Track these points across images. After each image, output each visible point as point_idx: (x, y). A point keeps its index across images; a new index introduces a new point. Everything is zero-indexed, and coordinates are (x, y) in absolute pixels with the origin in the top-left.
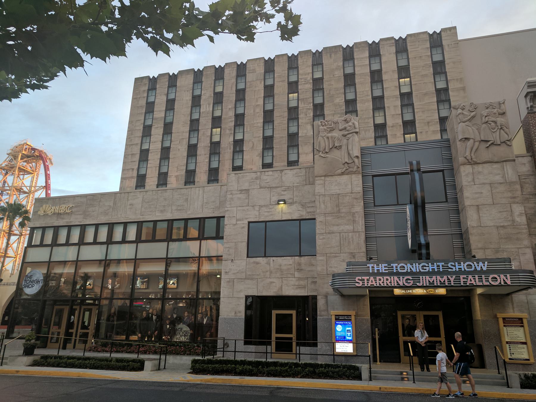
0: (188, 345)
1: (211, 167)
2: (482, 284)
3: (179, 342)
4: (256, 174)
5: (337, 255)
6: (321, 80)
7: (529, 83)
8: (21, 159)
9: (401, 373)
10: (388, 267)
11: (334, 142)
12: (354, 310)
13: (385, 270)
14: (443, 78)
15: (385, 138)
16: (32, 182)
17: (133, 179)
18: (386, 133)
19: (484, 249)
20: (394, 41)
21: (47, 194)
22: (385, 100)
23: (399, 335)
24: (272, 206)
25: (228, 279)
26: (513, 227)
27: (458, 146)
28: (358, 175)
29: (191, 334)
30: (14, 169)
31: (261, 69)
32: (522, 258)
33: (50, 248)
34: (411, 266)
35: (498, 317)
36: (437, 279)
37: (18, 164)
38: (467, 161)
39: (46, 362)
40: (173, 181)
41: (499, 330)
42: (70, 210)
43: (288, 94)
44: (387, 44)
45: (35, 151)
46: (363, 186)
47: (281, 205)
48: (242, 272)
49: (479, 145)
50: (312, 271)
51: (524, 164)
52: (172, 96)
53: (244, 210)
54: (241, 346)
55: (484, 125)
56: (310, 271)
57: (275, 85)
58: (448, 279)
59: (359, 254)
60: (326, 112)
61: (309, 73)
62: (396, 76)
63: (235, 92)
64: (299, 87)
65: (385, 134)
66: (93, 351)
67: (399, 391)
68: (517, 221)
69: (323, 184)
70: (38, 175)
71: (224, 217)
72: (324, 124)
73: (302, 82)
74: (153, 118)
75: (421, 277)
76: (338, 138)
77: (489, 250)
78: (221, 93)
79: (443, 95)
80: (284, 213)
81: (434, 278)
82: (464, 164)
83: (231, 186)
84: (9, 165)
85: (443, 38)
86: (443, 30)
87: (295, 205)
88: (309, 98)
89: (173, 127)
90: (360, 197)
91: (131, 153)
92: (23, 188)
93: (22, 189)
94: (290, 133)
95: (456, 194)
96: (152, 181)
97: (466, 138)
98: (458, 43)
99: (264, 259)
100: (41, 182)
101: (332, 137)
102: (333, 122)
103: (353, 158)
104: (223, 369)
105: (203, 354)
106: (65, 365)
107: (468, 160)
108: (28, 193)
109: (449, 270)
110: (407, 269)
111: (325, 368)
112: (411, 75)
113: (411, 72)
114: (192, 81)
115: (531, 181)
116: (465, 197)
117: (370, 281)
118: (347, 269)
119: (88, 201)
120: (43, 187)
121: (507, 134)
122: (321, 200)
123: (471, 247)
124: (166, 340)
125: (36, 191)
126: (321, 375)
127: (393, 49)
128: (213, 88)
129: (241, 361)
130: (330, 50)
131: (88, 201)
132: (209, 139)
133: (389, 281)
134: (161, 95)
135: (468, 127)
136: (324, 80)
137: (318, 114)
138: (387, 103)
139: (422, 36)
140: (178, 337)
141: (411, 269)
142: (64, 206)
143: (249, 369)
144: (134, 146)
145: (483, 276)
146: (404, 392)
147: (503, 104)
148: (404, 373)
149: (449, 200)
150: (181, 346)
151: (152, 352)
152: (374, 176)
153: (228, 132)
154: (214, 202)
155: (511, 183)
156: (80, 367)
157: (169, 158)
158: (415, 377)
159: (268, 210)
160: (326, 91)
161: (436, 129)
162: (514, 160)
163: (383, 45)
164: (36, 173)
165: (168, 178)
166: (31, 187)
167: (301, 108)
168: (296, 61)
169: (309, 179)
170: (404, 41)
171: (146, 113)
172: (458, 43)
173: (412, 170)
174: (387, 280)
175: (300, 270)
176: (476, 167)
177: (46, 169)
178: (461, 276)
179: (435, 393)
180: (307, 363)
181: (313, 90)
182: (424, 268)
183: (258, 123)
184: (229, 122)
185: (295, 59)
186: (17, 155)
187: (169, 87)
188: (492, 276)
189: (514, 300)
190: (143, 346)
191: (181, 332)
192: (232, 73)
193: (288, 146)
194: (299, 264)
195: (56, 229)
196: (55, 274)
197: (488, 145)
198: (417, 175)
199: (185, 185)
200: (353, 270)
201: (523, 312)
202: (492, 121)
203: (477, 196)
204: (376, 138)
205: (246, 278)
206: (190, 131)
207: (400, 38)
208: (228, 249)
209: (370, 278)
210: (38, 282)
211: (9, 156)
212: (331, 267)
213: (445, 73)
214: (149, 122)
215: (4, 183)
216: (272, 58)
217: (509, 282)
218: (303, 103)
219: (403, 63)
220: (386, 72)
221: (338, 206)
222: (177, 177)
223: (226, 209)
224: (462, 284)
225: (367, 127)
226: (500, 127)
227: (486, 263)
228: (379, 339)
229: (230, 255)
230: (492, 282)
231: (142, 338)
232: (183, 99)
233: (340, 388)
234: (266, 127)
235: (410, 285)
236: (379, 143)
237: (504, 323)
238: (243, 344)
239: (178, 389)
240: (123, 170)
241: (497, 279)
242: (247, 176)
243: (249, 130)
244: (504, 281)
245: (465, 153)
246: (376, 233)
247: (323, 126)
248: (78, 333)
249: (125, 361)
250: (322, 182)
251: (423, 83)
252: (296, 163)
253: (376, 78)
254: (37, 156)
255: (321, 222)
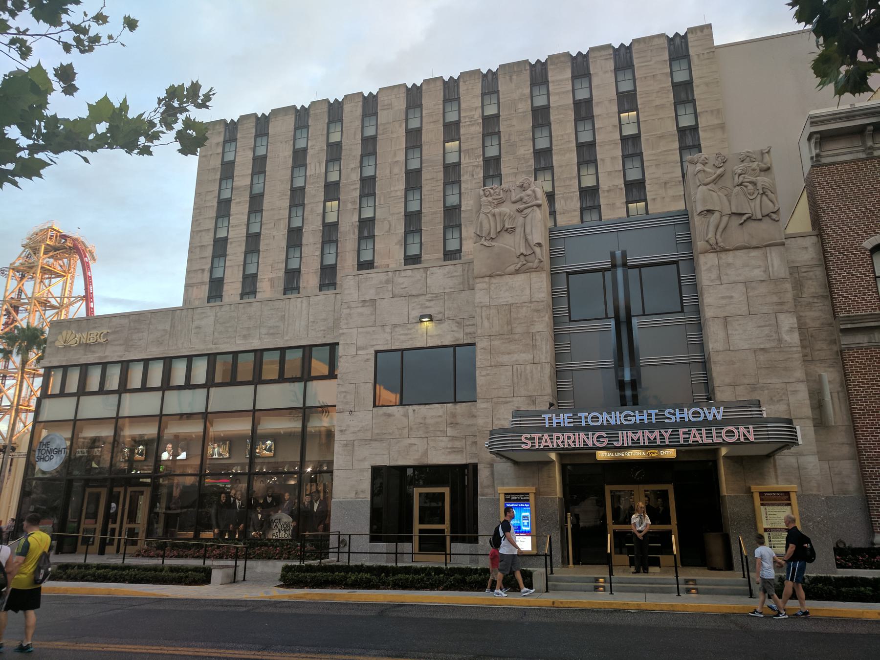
0: (288, 545)
1: (325, 263)
2: (711, 442)
3: (274, 540)
4: (387, 275)
5: (508, 399)
6: (495, 119)
7: (812, 118)
8: (45, 253)
9: (596, 580)
10: (574, 419)
11: (504, 221)
12: (533, 485)
13: (568, 423)
14: (690, 110)
15: (597, 210)
16: (64, 289)
17: (204, 286)
18: (599, 201)
19: (734, 385)
20: (611, 52)
21: (89, 310)
22: (597, 148)
23: (608, 522)
24: (412, 325)
25: (345, 442)
26: (778, 350)
27: (696, 223)
28: (541, 274)
29: (294, 527)
30: (33, 270)
31: (400, 104)
32: (792, 399)
33: (75, 399)
34: (608, 416)
35: (752, 491)
36: (643, 436)
37: (40, 261)
38: (709, 247)
39: (65, 574)
40: (265, 289)
41: (754, 510)
42: (103, 338)
43: (445, 142)
44: (601, 56)
45: (66, 240)
46: (552, 289)
47: (425, 323)
48: (367, 430)
49: (729, 220)
50: (472, 425)
51: (806, 248)
52: (261, 151)
53: (367, 333)
54: (361, 542)
55: (737, 189)
56: (469, 425)
57: (423, 128)
58: (661, 435)
59: (541, 397)
60: (504, 170)
61: (476, 108)
62: (615, 109)
63: (360, 142)
64: (462, 131)
65: (596, 204)
66: (143, 556)
67: (582, 606)
68: (786, 341)
69: (486, 289)
70: (73, 277)
71: (337, 344)
72: (488, 193)
73: (465, 122)
74: (232, 188)
75: (620, 432)
76: (510, 215)
77: (742, 387)
78: (339, 144)
79: (690, 137)
80: (430, 336)
81: (640, 433)
82: (706, 252)
83: (348, 294)
84: (26, 263)
85: (690, 44)
86: (691, 30)
87: (446, 323)
88: (477, 149)
89: (264, 201)
90: (544, 308)
91: (199, 244)
92: (49, 299)
93: (49, 302)
94: (447, 205)
95: (697, 299)
96: (232, 288)
97: (708, 211)
98: (714, 52)
99: (400, 408)
100: (79, 289)
101: (500, 214)
102: (502, 189)
103: (532, 246)
104: (328, 579)
105: (302, 558)
106: (93, 579)
107: (711, 245)
108: (59, 308)
109: (666, 421)
110: (603, 421)
111: (480, 575)
112: (639, 107)
113: (639, 102)
114: (292, 126)
115: (816, 276)
116: (705, 305)
117: (544, 440)
118: (513, 421)
119: (132, 324)
120: (81, 297)
121: (771, 201)
122: (483, 314)
123: (714, 383)
124: (257, 537)
125: (71, 304)
126: (474, 585)
127: (611, 65)
128: (326, 136)
129: (356, 566)
130: (508, 69)
131: (132, 324)
132: (320, 219)
133: (572, 439)
134: (244, 150)
135: (711, 192)
136: (500, 118)
137: (491, 173)
138: (601, 153)
139: (656, 42)
140: (275, 532)
141: (608, 421)
142: (95, 332)
143: (366, 578)
144: (203, 233)
145: (713, 429)
146: (588, 607)
147: (767, 154)
148: (601, 580)
149: (685, 309)
150: (277, 546)
151: (230, 555)
152: (569, 274)
153: (350, 206)
154: (325, 320)
155: (782, 280)
156: (116, 580)
157: (258, 251)
158: (612, 584)
159: (406, 332)
160: (504, 137)
161: (678, 194)
162: (783, 244)
163: (595, 57)
164: (69, 275)
165: (258, 284)
166: (62, 298)
167: (465, 166)
168: (456, 88)
169: (468, 281)
170: (628, 51)
171: (221, 180)
172: (714, 51)
173: (614, 266)
174: (569, 438)
175: (454, 425)
176: (723, 255)
177: (86, 268)
178: (680, 430)
179: (755, 611)
180: (454, 568)
181: (484, 136)
182: (629, 418)
183: (396, 191)
184: (351, 191)
185: (454, 86)
186: (38, 248)
187: (256, 136)
188: (726, 429)
189: (777, 464)
190: (219, 547)
191: (280, 525)
192: (356, 111)
193: (444, 227)
194: (454, 415)
195: (84, 369)
196: (84, 438)
197: (742, 221)
198: (620, 272)
199: (284, 294)
200: (521, 424)
201: (791, 483)
202: (750, 182)
203: (724, 302)
204: (582, 210)
205: (371, 440)
206: (291, 207)
207: (622, 45)
208: (345, 394)
209: (543, 436)
210: (58, 451)
211: (25, 249)
212: (499, 419)
213: (693, 101)
214: (226, 195)
215: (19, 292)
216: (419, 85)
217: (752, 438)
218: (467, 157)
219: (626, 87)
220: (598, 103)
221: (509, 323)
222: (271, 280)
223: (341, 331)
224: (682, 442)
225: (568, 193)
226: (761, 192)
227: (722, 408)
228: (572, 529)
229: (347, 403)
230: (727, 438)
231: (221, 534)
232: (278, 155)
233: (495, 603)
234: (410, 198)
235: (604, 445)
236: (587, 218)
237: (761, 500)
238: (368, 540)
239: (245, 609)
240: (188, 272)
241: (734, 433)
242: (372, 278)
243: (382, 202)
244: (745, 435)
245: (707, 234)
246: (572, 364)
247: (486, 197)
248: (124, 528)
249: (183, 570)
250: (485, 286)
251: (658, 119)
252: (458, 254)
253: (583, 114)
254: (70, 247)
255: (483, 348)
